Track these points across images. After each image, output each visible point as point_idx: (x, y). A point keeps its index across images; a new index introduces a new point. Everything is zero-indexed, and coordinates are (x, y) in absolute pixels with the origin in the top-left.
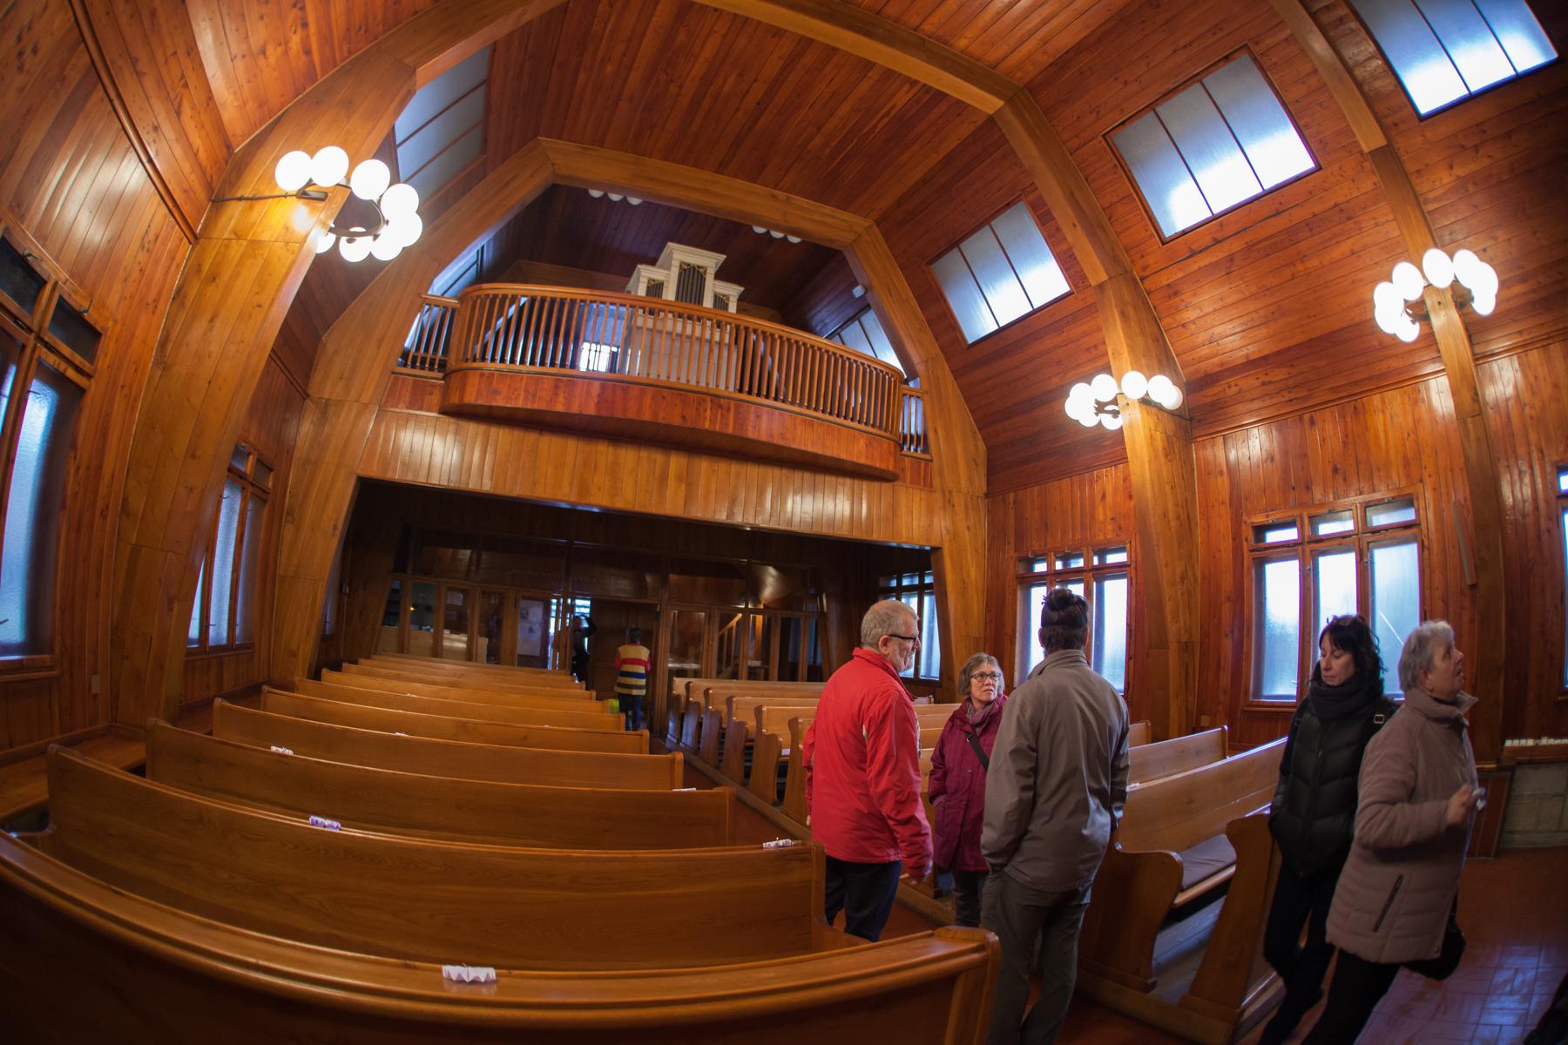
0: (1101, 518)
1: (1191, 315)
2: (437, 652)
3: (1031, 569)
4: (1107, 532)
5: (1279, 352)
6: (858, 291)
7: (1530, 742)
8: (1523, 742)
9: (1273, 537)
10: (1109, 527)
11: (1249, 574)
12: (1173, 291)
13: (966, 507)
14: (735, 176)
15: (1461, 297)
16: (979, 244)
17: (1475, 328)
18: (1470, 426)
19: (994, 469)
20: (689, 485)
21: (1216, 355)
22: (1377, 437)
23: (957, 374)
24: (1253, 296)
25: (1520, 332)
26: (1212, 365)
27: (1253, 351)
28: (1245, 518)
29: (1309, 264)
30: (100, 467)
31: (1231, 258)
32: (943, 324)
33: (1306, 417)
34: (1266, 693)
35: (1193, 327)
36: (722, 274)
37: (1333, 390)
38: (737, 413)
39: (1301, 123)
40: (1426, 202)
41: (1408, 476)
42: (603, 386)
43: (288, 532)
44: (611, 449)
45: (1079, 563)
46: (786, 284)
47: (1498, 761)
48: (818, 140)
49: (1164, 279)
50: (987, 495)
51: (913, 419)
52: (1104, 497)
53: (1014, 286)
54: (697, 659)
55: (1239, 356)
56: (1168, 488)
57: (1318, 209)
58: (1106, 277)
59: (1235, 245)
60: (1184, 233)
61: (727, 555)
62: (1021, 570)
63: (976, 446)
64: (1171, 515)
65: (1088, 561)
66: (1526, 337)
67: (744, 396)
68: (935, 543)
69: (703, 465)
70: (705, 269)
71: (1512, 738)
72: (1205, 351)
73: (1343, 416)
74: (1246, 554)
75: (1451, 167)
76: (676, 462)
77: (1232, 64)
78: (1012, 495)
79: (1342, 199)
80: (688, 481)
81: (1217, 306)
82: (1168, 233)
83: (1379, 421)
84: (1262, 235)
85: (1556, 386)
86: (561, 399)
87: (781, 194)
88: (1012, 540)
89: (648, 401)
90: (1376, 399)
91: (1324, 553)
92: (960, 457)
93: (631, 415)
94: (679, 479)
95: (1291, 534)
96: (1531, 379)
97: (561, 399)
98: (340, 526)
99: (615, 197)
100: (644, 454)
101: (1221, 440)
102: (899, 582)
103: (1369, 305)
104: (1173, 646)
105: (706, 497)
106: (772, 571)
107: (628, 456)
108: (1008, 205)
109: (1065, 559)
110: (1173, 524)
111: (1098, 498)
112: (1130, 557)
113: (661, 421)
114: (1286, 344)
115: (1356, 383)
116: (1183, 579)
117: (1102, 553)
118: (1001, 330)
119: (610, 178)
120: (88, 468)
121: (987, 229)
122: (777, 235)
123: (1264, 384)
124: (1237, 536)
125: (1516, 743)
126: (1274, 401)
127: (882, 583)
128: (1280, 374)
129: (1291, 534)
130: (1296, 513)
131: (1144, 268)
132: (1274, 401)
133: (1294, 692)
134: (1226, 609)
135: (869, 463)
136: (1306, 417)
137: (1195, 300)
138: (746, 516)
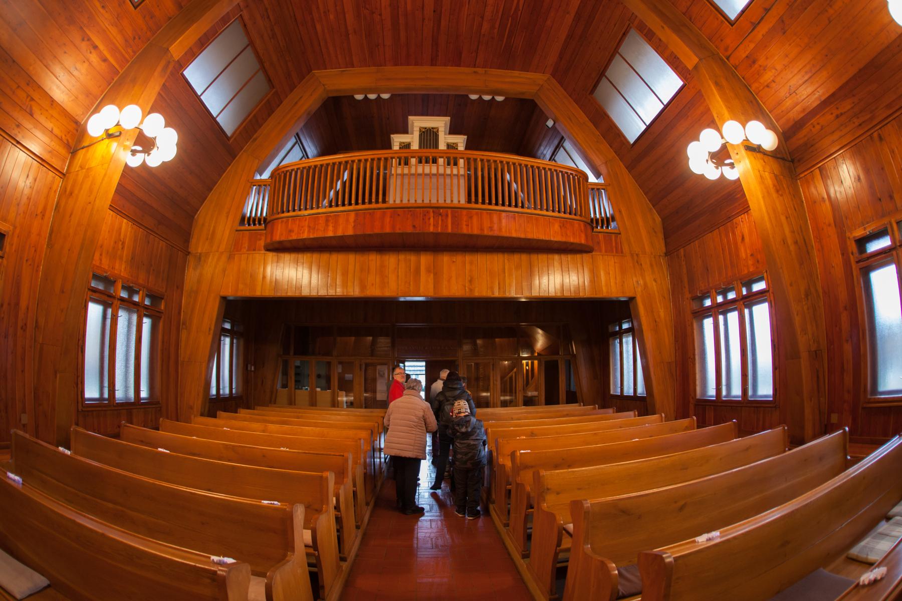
0: (743, 255)
1: (768, 76)
2: (335, 404)
3: (702, 304)
4: (749, 267)
6: (550, 123)
9: (874, 246)
10: (750, 262)
11: (859, 283)
12: (751, 60)
13: (651, 265)
14: (445, 65)
16: (617, 69)
19: (668, 234)
20: (435, 274)
23: (630, 168)
26: (795, 114)
28: (848, 234)
30: (17, 304)
32: (610, 132)
33: (875, 135)
34: (881, 388)
35: (773, 85)
36: (453, 130)
37: (889, 106)
38: (453, 217)
42: (357, 215)
43: (184, 335)
44: (379, 257)
45: (731, 296)
46: (510, 129)
48: (486, 26)
49: (742, 53)
50: (666, 254)
51: (603, 207)
52: (743, 238)
53: (647, 92)
54: (511, 394)
56: (783, 218)
58: (696, 60)
60: (743, 12)
61: (510, 319)
62: (695, 306)
63: (654, 220)
64: (790, 241)
65: (739, 292)
67: (473, 205)
68: (631, 295)
69: (445, 259)
70: (437, 129)
72: (788, 103)
74: (854, 267)
76: (425, 259)
78: (682, 251)
80: (436, 272)
82: (733, 16)
86: (331, 228)
87: (480, 70)
88: (687, 286)
89: (388, 220)
92: (643, 229)
93: (377, 231)
94: (428, 271)
95: (884, 243)
97: (331, 228)
98: (213, 328)
99: (372, 96)
100: (402, 257)
102: (620, 327)
104: (804, 355)
105: (449, 281)
106: (540, 331)
107: (391, 260)
108: (624, 34)
109: (724, 293)
110: (792, 248)
111: (739, 239)
112: (768, 284)
113: (398, 231)
114: (844, 79)
116: (807, 295)
117: (748, 285)
118: (649, 127)
119: (362, 83)
120: (9, 304)
121: (617, 55)
122: (487, 98)
123: (837, 117)
127: (611, 329)
128: (847, 105)
129: (884, 243)
130: (885, 221)
131: (726, 49)
134: (844, 318)
135: (564, 240)
136: (875, 135)
138: (515, 291)
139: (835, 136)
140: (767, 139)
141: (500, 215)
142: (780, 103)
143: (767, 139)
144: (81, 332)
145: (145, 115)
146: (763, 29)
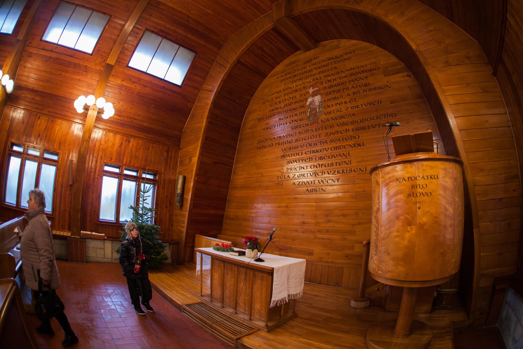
1: (29, 65)
5: (41, 92)
7: (89, 233)
8: (87, 232)
9: (15, 148)
12: (30, 55)
15: (101, 111)
17: (99, 119)
18: (85, 143)
21: (26, 82)
22: (55, 131)
24: (47, 72)
25: (110, 127)
27: (36, 87)
29: (66, 75)
31: (50, 58)
33: (38, 115)
37: (49, 112)
39: (100, 42)
40: (109, 83)
41: (59, 147)
47: (80, 236)
55: (31, 86)
57: (81, 63)
58: (21, 39)
59: (54, 55)
66: (111, 128)
71: (83, 231)
72: (24, 78)
73: (48, 120)
75: (123, 81)
77: (103, 15)
79: (89, 66)
81: (37, 68)
82: (44, 39)
83: (57, 128)
84: (66, 60)
85: (114, 144)
90: (60, 121)
91: (29, 160)
96: (107, 139)
101: (13, 109)
103: (77, 96)
115: (56, 113)
123: (32, 98)
124: (6, 144)
125: (84, 232)
126: (32, 105)
128: (38, 98)
129: (20, 150)
132: (32, 105)
133: (50, 210)
136: (38, 115)
137: (33, 62)
139: (26, 103)
140: (10, 88)
141: (254, 275)
142: (22, 76)
143: (10, 88)
144: (162, 84)
145: (96, 99)
146: (43, 53)
